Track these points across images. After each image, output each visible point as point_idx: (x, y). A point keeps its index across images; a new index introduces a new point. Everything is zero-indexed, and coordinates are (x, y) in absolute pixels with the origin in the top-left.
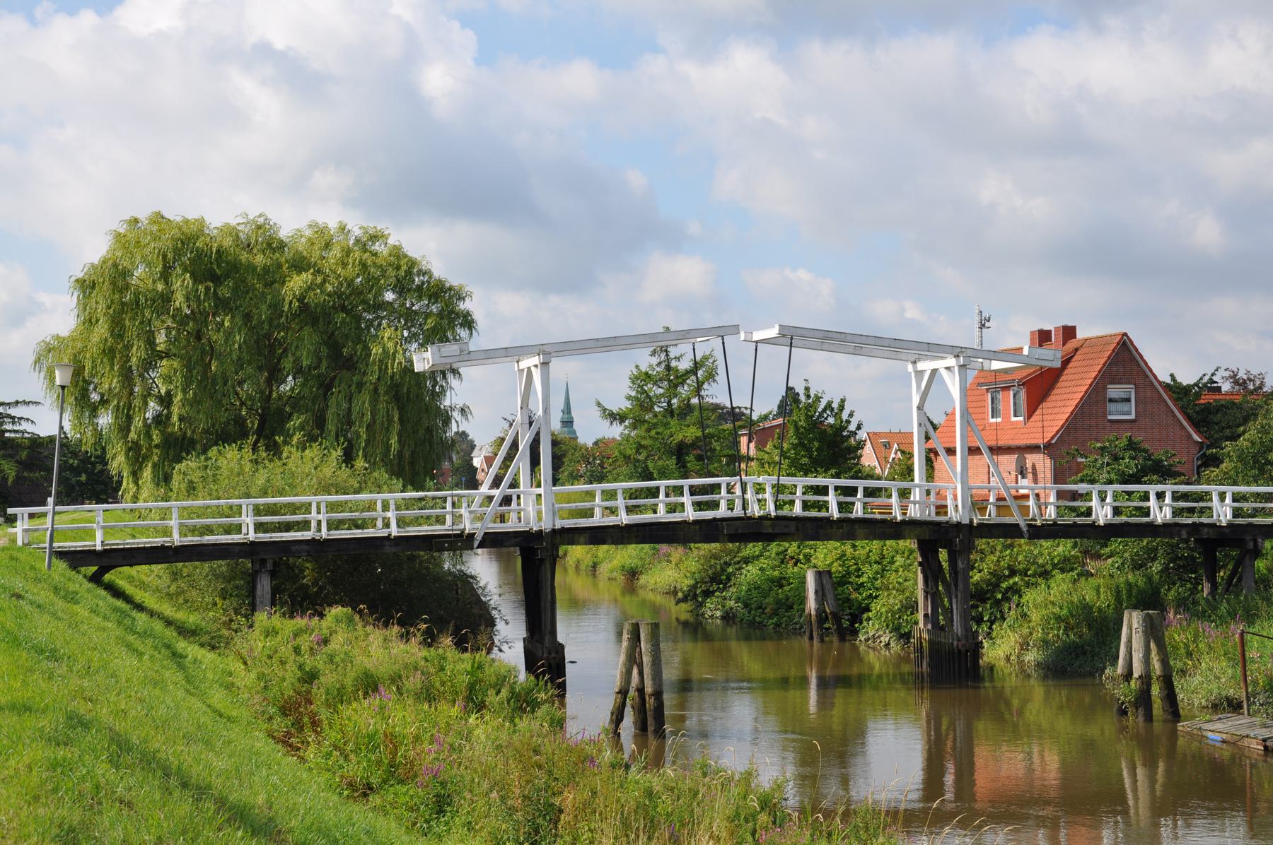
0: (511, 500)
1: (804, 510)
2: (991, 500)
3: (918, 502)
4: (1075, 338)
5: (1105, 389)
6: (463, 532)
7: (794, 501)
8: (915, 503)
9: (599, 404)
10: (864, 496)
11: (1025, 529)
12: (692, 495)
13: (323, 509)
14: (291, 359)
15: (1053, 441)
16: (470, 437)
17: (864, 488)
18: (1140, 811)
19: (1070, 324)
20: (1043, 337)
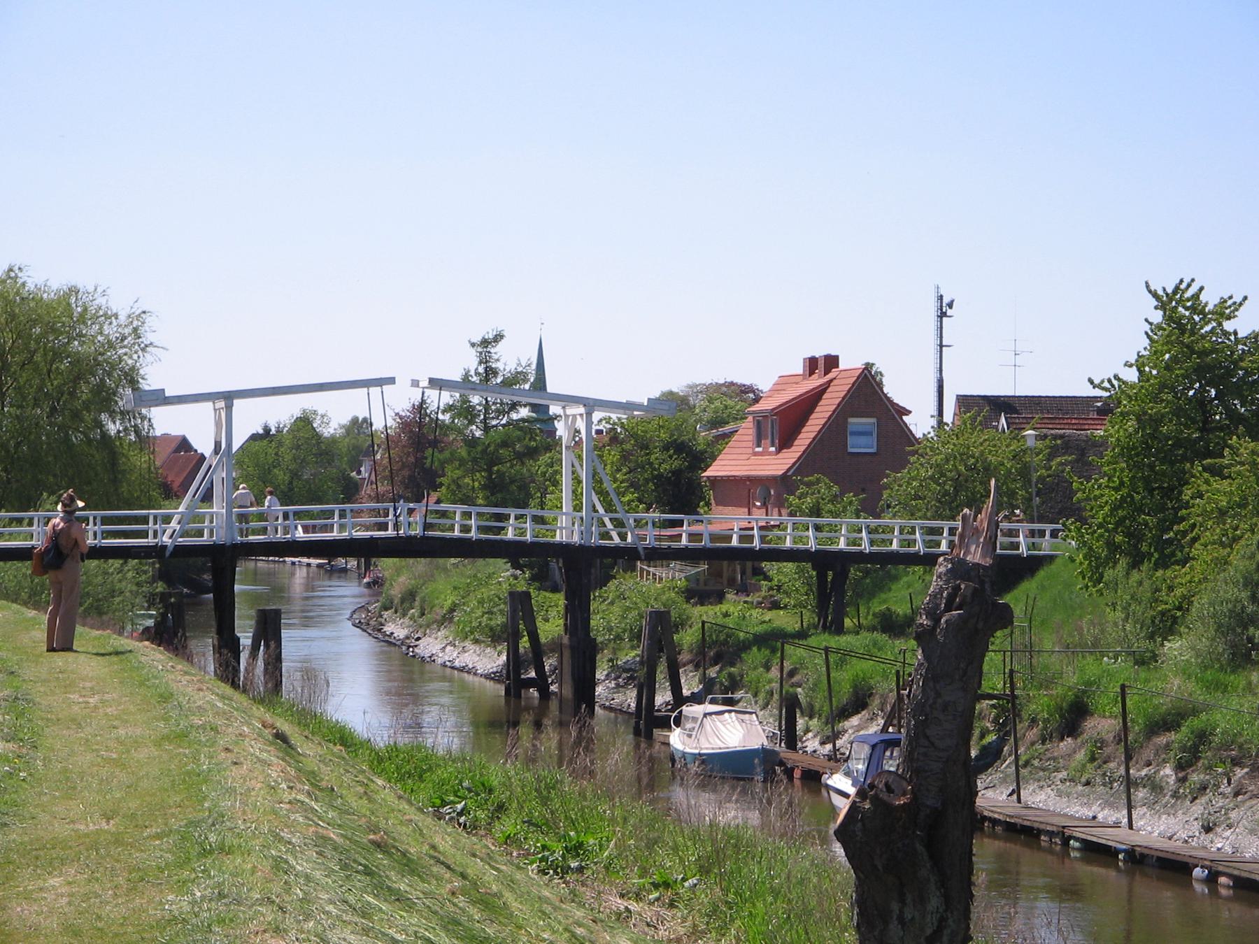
0: (465, 525)
1: (740, 543)
2: (735, 530)
3: (564, 528)
4: (838, 367)
5: (846, 422)
6: (157, 545)
7: (681, 535)
8: (561, 528)
9: (1146, 320)
10: (949, 535)
11: (642, 552)
12: (870, 533)
13: (98, 522)
14: (49, 358)
15: (790, 473)
16: (199, 452)
17: (950, 528)
18: (63, 594)
19: (833, 353)
20: (812, 364)
